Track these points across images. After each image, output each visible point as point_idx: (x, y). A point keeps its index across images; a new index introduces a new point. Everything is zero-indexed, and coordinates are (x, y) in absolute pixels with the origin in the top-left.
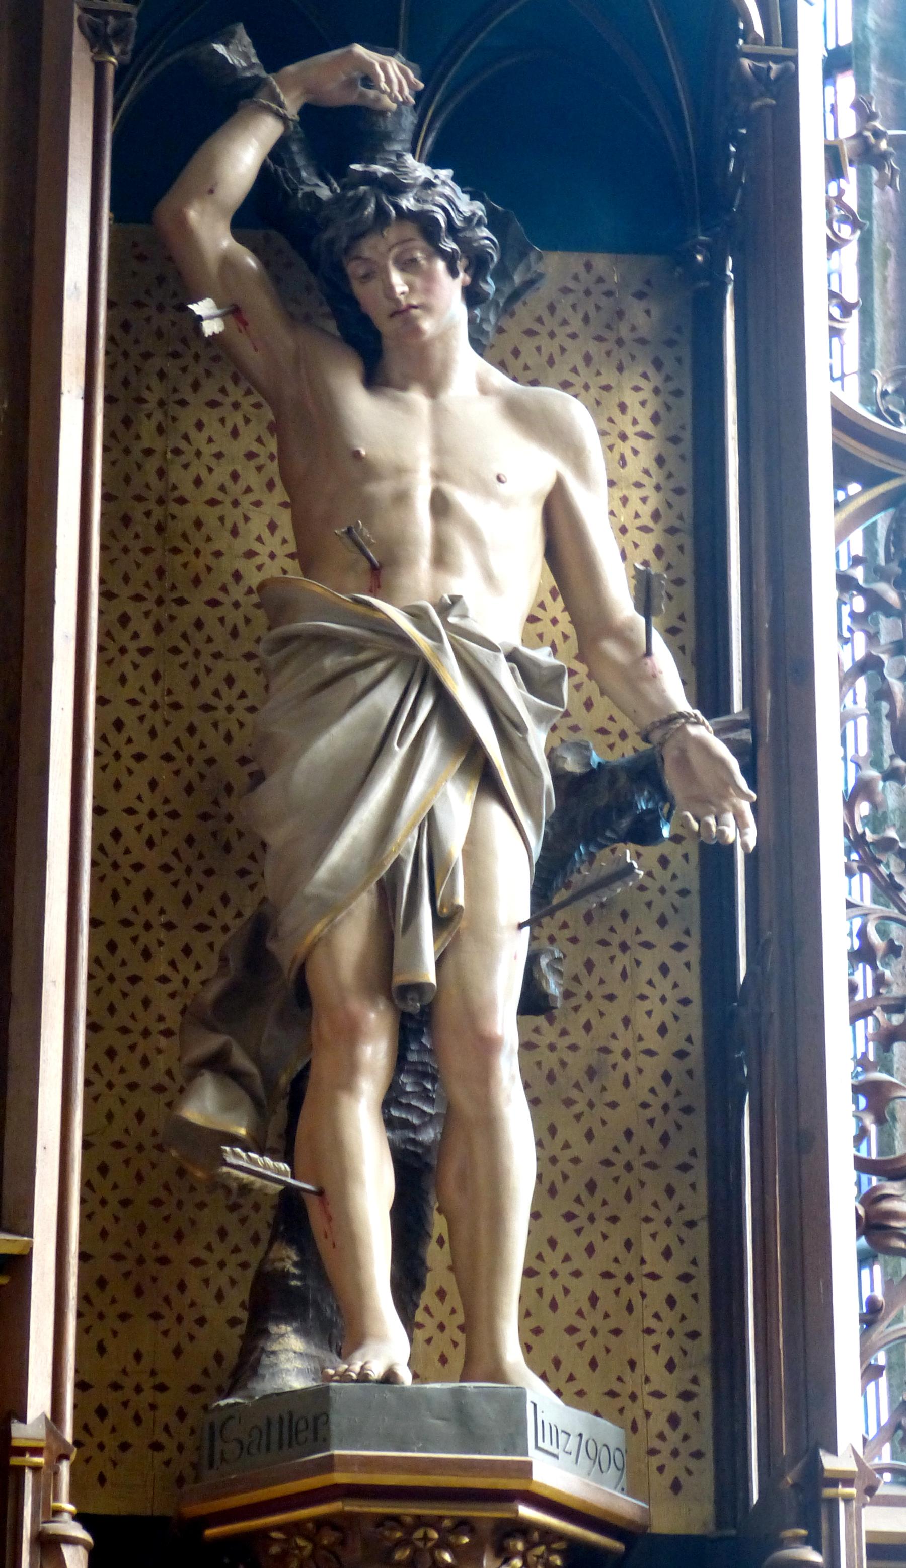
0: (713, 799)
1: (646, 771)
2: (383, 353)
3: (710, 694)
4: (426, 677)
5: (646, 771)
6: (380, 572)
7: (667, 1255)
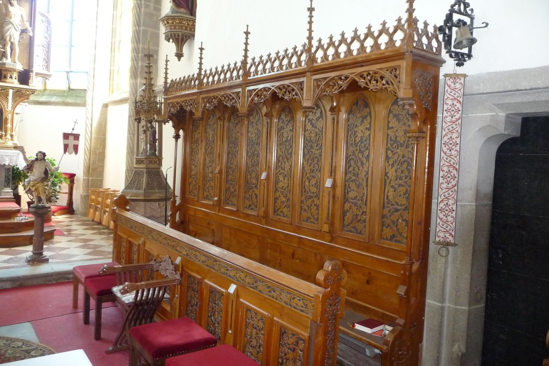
0: (30, 32)
1: (26, 30)
2: (11, 4)
3: (31, 26)
4: (13, 25)
5: (26, 30)
6: (11, 18)
7: (26, 55)
